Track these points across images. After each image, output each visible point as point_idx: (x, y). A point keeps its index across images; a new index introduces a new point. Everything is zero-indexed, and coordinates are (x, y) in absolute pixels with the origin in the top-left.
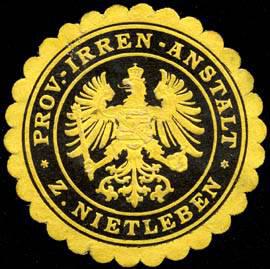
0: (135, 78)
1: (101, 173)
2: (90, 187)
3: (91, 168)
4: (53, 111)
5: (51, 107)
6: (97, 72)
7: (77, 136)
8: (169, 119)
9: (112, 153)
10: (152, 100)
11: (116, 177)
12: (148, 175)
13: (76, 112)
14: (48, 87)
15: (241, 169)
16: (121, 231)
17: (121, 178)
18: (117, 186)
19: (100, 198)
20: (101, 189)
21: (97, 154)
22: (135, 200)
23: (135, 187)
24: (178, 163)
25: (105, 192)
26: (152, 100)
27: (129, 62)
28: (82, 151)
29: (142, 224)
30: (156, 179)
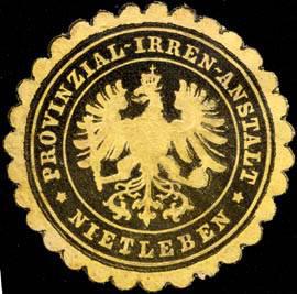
0: (149, 86)
1: (109, 189)
2: (97, 199)
3: (100, 182)
4: (58, 145)
5: (54, 141)
6: (111, 79)
7: (88, 149)
8: (200, 129)
9: (124, 171)
10: (171, 113)
11: (127, 192)
12: (166, 191)
13: (86, 124)
14: (45, 123)
15: (256, 207)
16: (114, 247)
17: (133, 193)
18: (129, 200)
19: (109, 214)
20: (110, 203)
21: (109, 167)
22: (146, 217)
23: (148, 201)
24: (198, 180)
25: (113, 207)
26: (171, 113)
27: (145, 68)
28: (93, 162)
29: (137, 243)
30: (173, 195)
